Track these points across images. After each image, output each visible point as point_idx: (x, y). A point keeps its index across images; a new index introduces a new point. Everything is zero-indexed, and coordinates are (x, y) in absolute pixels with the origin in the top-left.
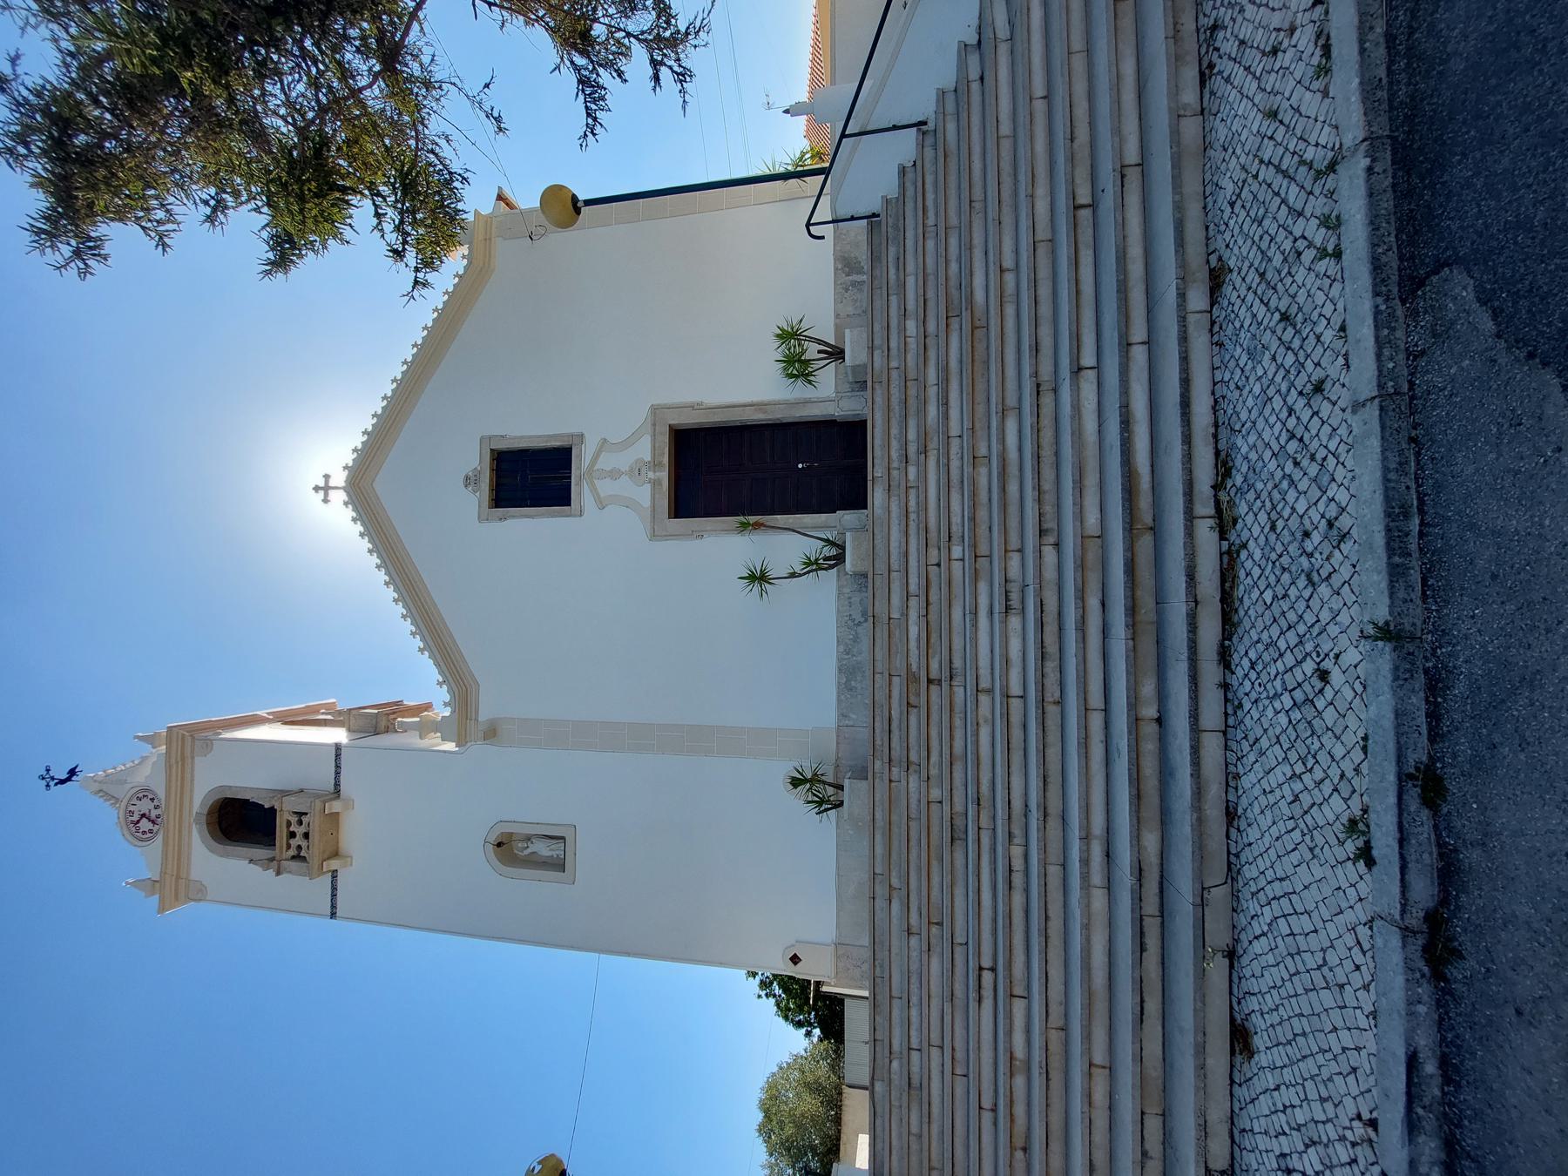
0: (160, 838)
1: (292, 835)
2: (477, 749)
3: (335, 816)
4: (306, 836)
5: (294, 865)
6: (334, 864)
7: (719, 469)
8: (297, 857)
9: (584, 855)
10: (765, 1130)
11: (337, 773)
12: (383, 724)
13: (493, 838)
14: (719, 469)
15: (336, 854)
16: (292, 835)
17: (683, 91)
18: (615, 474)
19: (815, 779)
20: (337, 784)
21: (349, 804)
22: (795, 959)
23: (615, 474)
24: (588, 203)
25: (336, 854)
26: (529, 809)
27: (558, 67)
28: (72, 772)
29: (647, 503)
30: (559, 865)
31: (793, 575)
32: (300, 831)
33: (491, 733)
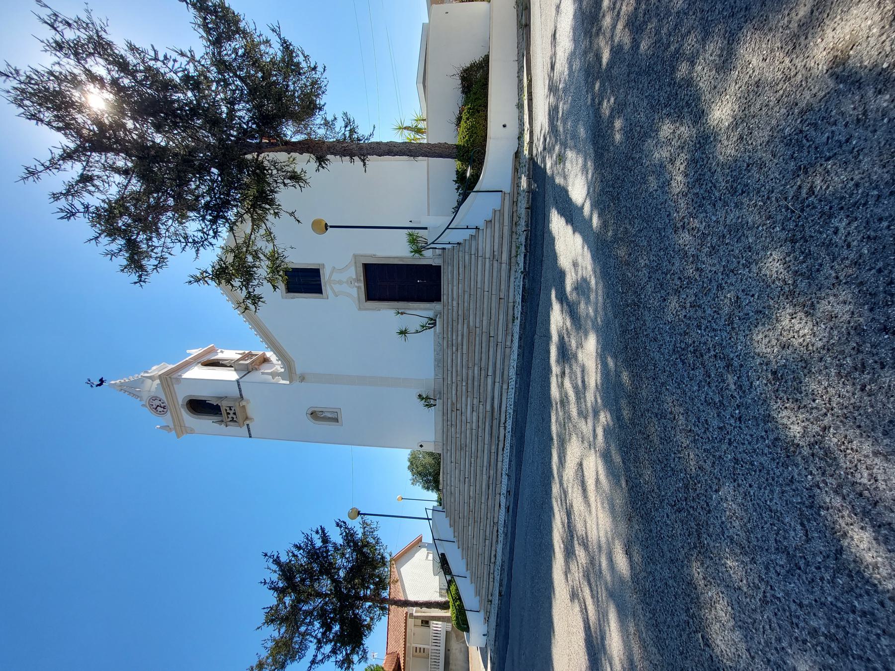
0: (169, 413)
1: (229, 414)
2: (297, 384)
3: (244, 406)
4: (235, 414)
5: (232, 423)
6: (248, 422)
7: (386, 283)
8: (233, 420)
9: (344, 417)
10: (411, 468)
11: (240, 391)
12: (250, 368)
13: (310, 412)
14: (386, 283)
15: (247, 418)
16: (229, 414)
17: (364, 165)
18: (340, 282)
19: (427, 398)
20: (241, 395)
21: (248, 401)
22: (421, 446)
23: (340, 282)
24: (331, 227)
25: (247, 418)
26: (321, 403)
27: (309, 161)
28: (102, 381)
29: (356, 295)
30: (336, 420)
31: (417, 332)
32: (231, 412)
33: (303, 379)
